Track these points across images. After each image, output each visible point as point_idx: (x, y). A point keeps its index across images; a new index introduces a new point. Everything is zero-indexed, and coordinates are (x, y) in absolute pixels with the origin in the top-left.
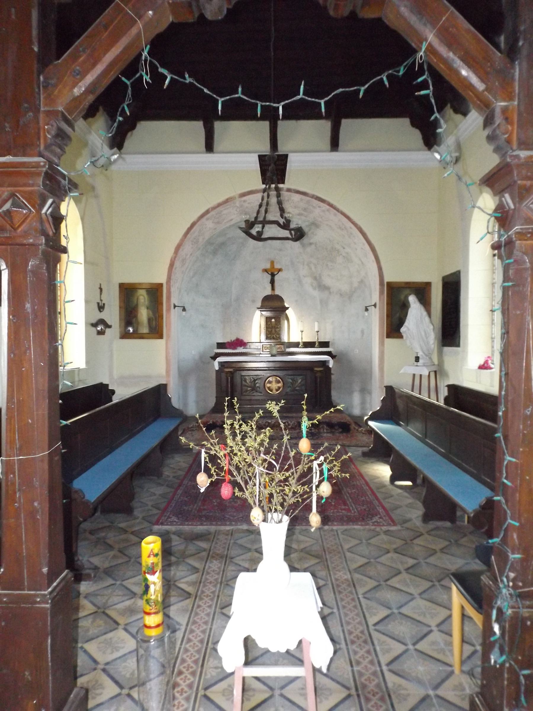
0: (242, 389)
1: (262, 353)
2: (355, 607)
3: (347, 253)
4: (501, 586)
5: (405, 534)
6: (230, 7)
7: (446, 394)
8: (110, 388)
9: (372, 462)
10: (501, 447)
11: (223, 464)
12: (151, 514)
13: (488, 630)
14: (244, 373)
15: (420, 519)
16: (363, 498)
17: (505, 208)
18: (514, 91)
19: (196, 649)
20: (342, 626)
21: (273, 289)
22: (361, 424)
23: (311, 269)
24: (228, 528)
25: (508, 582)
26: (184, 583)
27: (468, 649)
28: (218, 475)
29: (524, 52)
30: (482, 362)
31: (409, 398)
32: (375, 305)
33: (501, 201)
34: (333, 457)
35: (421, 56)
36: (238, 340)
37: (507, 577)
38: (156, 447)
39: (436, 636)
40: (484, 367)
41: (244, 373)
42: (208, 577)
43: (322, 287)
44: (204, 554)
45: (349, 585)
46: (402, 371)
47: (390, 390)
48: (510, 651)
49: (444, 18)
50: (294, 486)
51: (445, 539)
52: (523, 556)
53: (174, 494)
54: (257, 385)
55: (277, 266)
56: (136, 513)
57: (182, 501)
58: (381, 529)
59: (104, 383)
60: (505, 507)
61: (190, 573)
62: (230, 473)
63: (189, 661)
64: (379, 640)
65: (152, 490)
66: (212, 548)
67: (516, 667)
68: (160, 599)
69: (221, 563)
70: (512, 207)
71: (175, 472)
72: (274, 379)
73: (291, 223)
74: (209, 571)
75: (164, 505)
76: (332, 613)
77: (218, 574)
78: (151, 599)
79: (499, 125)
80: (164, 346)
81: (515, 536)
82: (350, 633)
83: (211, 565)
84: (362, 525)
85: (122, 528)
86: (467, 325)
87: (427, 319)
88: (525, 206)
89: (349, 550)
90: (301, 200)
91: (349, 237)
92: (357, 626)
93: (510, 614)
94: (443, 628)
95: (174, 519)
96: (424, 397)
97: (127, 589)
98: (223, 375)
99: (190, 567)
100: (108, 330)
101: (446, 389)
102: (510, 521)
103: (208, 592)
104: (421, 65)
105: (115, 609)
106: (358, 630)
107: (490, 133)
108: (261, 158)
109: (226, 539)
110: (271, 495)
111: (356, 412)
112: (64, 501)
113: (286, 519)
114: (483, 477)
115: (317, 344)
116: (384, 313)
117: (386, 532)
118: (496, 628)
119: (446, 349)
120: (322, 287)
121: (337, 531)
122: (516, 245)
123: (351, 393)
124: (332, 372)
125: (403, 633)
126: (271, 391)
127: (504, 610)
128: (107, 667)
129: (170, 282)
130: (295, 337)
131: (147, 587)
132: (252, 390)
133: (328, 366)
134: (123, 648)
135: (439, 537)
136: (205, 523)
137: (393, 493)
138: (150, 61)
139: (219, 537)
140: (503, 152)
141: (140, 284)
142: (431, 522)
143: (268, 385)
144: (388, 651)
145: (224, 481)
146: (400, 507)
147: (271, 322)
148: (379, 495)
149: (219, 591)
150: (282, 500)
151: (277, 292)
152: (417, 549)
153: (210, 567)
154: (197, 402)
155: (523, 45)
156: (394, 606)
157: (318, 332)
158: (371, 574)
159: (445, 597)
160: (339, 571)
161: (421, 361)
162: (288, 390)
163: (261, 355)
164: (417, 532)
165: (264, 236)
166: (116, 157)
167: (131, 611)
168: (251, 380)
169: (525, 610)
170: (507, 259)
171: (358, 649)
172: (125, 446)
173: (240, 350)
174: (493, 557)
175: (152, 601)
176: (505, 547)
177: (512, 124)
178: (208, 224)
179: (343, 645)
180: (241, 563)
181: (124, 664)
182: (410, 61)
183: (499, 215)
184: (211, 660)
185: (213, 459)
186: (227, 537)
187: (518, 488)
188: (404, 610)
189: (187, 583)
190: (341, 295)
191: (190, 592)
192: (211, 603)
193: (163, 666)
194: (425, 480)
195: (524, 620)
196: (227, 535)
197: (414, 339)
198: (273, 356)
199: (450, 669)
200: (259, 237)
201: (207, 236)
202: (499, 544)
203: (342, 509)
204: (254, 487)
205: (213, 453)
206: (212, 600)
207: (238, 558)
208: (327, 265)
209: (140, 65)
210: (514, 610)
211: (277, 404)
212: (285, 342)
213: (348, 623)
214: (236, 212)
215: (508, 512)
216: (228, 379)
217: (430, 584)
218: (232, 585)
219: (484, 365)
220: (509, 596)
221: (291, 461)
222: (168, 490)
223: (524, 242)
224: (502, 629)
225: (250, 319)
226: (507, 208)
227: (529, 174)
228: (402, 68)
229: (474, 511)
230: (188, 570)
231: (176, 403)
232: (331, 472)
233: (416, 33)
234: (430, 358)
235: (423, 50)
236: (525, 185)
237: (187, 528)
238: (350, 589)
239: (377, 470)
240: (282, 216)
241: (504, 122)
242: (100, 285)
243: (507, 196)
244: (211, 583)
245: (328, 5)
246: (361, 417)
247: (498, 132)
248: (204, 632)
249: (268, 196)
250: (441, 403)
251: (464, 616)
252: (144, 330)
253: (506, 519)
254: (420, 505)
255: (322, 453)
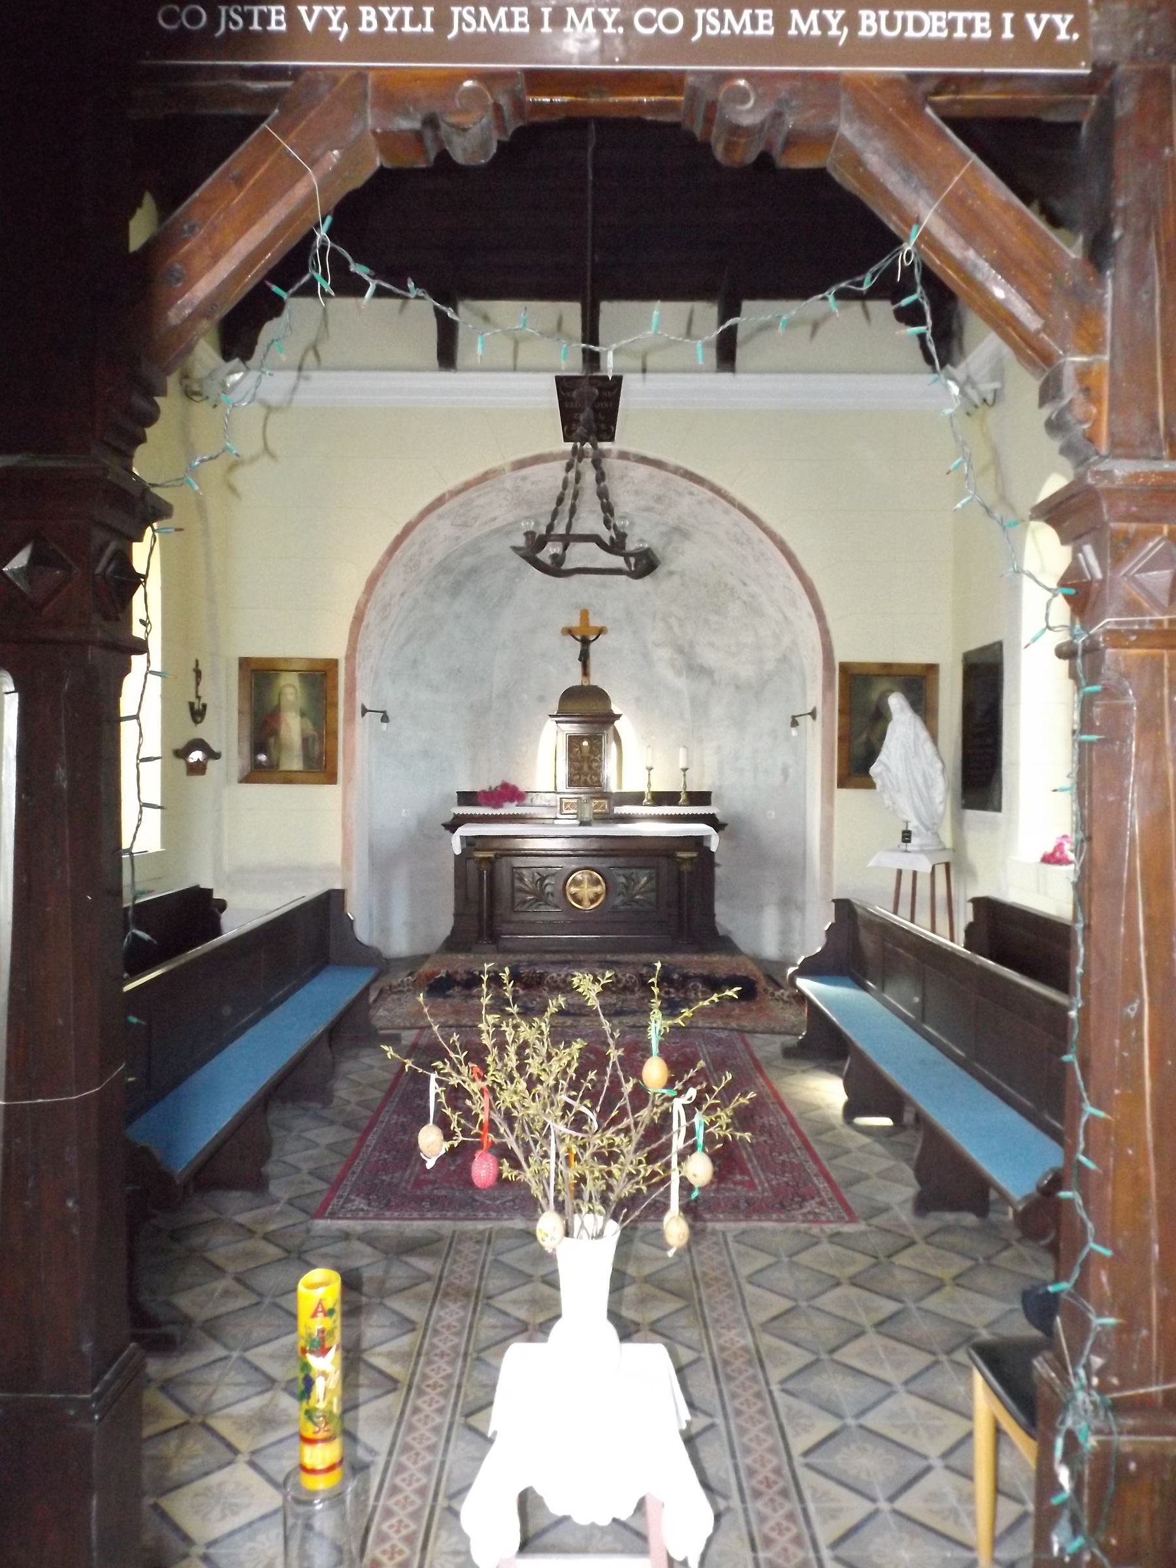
0: (513, 897)
1: (559, 816)
2: (763, 1412)
3: (753, 596)
4: (1075, 1384)
5: (876, 1241)
6: (505, 139)
7: (970, 918)
8: (216, 896)
9: (804, 1071)
10: (1076, 1086)
11: (476, 1109)
12: (308, 1191)
13: (1046, 1482)
14: (518, 862)
15: (909, 1206)
16: (783, 1157)
17: (1085, 577)
18: (1103, 333)
19: (410, 1509)
20: (733, 1456)
21: (585, 672)
22: (780, 980)
23: (670, 628)
24: (481, 1226)
25: (1089, 1379)
26: (380, 1354)
27: (1009, 1511)
28: (465, 1132)
29: (1125, 252)
30: (1050, 850)
31: (886, 929)
32: (813, 714)
33: (1075, 558)
34: (715, 1098)
35: (909, 255)
36: (505, 786)
37: (1087, 1367)
38: (320, 1037)
39: (939, 1480)
40: (1052, 859)
41: (518, 862)
42: (435, 1340)
43: (696, 670)
44: (428, 1287)
45: (750, 1363)
46: (871, 864)
47: (844, 908)
48: (1093, 1529)
49: (956, 178)
50: (630, 1159)
51: (962, 1254)
52: (1120, 1321)
53: (362, 1140)
54: (548, 889)
55: (595, 622)
56: (274, 1188)
57: (377, 1162)
58: (822, 1230)
59: (202, 886)
60: (1084, 1215)
61: (394, 1331)
62: (492, 1127)
63: (396, 1539)
64: (814, 1490)
65: (310, 1135)
66: (446, 1273)
67: (1105, 1561)
68: (336, 1409)
69: (464, 1307)
70: (1099, 575)
71: (361, 1094)
72: (586, 876)
73: (627, 541)
74: (438, 1327)
75: (337, 1170)
76: (712, 1426)
77: (459, 1334)
78: (316, 1409)
79: (1071, 402)
80: (339, 805)
81: (1104, 1278)
82: (751, 1472)
83: (442, 1313)
84: (778, 1220)
85: (241, 1225)
86: (1015, 764)
87: (928, 746)
88: (1125, 575)
89: (751, 1280)
90: (651, 477)
91: (757, 561)
92: (768, 1456)
93: (1093, 1447)
94: (955, 1461)
95: (359, 1203)
96: (921, 928)
97: (257, 1369)
98: (471, 865)
99: (395, 1318)
100: (212, 765)
101: (970, 906)
102: (1092, 1245)
103: (435, 1378)
104: (908, 272)
105: (230, 1417)
106: (770, 1466)
107: (1054, 416)
108: (564, 385)
109: (477, 1252)
110: (582, 1179)
111: (770, 949)
112: (129, 1188)
113: (613, 1229)
114: (1047, 1117)
115: (683, 797)
116: (833, 735)
117: (835, 1237)
118: (1064, 1475)
119: (972, 815)
120: (696, 670)
121: (724, 1234)
122: (1107, 656)
123: (758, 908)
124: (717, 860)
125: (868, 1474)
126: (579, 902)
127: (1081, 1439)
128: (212, 1551)
129: (354, 658)
130: (634, 783)
131: (309, 1383)
132: (537, 901)
133: (708, 848)
134: (248, 1506)
135: (951, 1248)
136: (429, 1215)
137: (851, 1145)
138: (332, 249)
139: (460, 1247)
140: (1082, 457)
141: (286, 660)
142: (933, 1214)
143: (573, 890)
144: (834, 1514)
145: (479, 1146)
146: (866, 1177)
147: (581, 747)
148: (817, 1149)
149: (462, 1374)
150: (604, 1187)
151: (595, 680)
152: (900, 1275)
153: (440, 1319)
154: (412, 926)
155: (1121, 238)
156: (848, 1410)
157: (685, 770)
158: (801, 1335)
159: (962, 1389)
160: (729, 1328)
161: (915, 840)
162: (618, 901)
163: (556, 822)
164: (902, 1236)
165: (567, 566)
166: (237, 377)
167: (266, 1421)
168: (533, 877)
169: (1124, 1438)
170: (1088, 685)
171: (767, 1511)
172: (252, 1032)
173: (510, 809)
174: (1058, 1319)
175: (318, 1414)
176: (1082, 1300)
177: (1097, 401)
178: (442, 529)
179: (735, 1501)
180: (510, 1309)
181: (250, 1545)
182: (885, 263)
183: (1072, 591)
184: (444, 1534)
185: (456, 1095)
186: (478, 1247)
187: (1111, 1174)
188: (870, 1420)
189: (388, 1354)
190: (738, 687)
191: (396, 1375)
192: (442, 1402)
193: (339, 1550)
194: (921, 1119)
195: (1123, 1459)
196: (478, 1242)
197: (899, 791)
198: (582, 824)
199: (966, 1555)
200: (556, 569)
201: (439, 554)
202: (1069, 1294)
203: (735, 1183)
204: (545, 1161)
205: (454, 1081)
206: (445, 1394)
207: (501, 1298)
208: (706, 621)
209: (311, 258)
210: (1102, 1438)
211: (596, 981)
212: (611, 793)
213: (747, 1451)
214: (505, 503)
215: (1090, 1225)
216: (481, 874)
217: (931, 1359)
218: (493, 1362)
219: (1052, 855)
220: (1090, 1407)
221: (625, 1101)
222: (348, 1134)
223: (1123, 651)
224: (1076, 1477)
225: (534, 736)
226: (1089, 577)
227: (1134, 509)
228: (868, 277)
229: (1026, 1198)
230: (392, 1325)
231: (363, 933)
232: (711, 1129)
233: (897, 207)
234: (936, 834)
235: (913, 241)
236: (1126, 532)
237: (388, 1226)
238: (751, 1371)
239: (815, 1089)
240: (607, 523)
241: (1081, 396)
242: (197, 662)
243: (1088, 549)
244: (442, 1355)
245: (713, 141)
246: (783, 964)
247: (1069, 417)
248: (427, 1470)
249: (578, 479)
250: (959, 946)
251: (998, 1432)
252: (293, 762)
253: (1084, 1243)
254: (909, 1173)
255: (692, 1082)
